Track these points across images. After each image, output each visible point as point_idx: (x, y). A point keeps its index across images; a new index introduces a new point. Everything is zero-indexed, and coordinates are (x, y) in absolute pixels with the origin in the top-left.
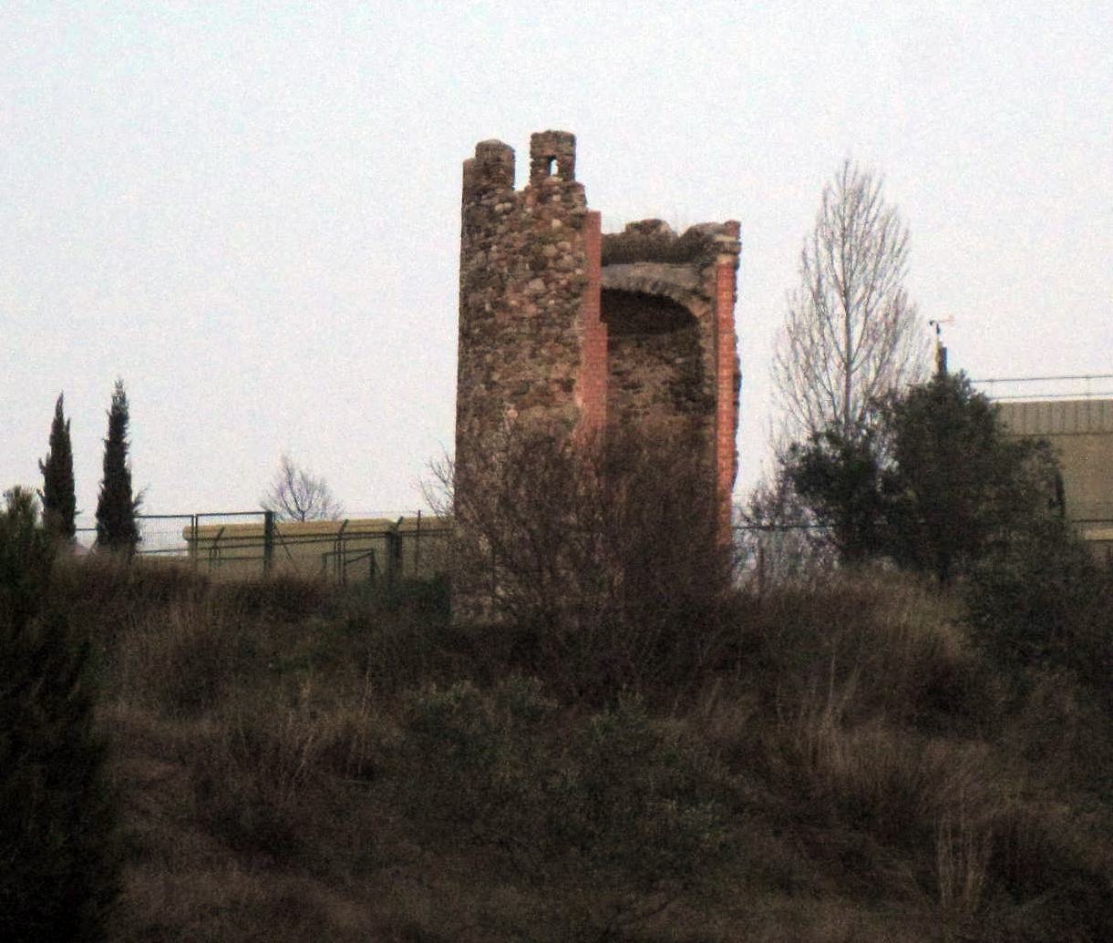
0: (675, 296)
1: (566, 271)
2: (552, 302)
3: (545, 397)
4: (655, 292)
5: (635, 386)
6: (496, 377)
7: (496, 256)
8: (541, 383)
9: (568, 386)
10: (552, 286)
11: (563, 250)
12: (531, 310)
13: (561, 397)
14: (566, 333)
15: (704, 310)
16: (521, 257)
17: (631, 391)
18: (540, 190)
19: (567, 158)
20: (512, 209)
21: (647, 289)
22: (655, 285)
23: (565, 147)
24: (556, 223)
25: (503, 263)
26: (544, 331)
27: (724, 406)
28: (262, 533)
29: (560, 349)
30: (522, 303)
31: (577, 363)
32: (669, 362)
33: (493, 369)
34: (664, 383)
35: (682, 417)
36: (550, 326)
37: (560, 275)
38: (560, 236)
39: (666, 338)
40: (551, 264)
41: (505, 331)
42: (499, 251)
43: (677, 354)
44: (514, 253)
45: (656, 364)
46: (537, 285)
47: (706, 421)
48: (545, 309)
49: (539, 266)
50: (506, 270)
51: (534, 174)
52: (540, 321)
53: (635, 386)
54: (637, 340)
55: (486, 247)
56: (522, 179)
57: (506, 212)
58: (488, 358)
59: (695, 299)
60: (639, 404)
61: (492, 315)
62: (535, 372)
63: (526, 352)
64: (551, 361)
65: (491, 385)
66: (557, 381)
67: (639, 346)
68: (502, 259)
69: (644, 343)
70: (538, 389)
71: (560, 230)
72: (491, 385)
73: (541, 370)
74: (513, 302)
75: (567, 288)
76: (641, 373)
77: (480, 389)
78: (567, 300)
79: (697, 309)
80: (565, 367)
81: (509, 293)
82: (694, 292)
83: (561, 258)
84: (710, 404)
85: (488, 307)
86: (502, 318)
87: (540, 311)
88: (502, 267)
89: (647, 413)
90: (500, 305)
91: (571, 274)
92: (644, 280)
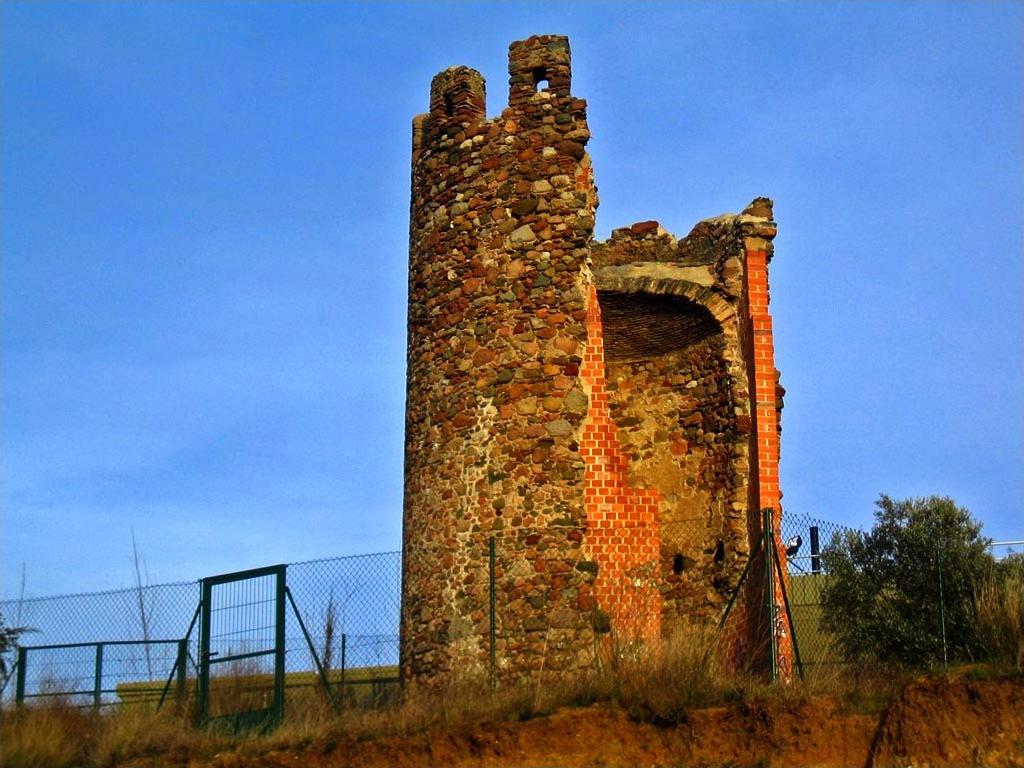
0: (691, 295)
1: (564, 213)
2: (547, 255)
3: (539, 383)
4: (663, 291)
5: (634, 422)
6: (465, 365)
7: (463, 206)
8: (532, 365)
9: (571, 367)
10: (546, 234)
11: (561, 185)
12: (516, 268)
13: (564, 383)
14: (566, 295)
15: (727, 313)
16: (500, 201)
17: (627, 428)
18: (527, 115)
19: (561, 67)
20: (486, 142)
21: (652, 288)
22: (661, 284)
23: (557, 54)
24: (549, 151)
25: (473, 214)
26: (535, 293)
27: (765, 428)
28: (396, 675)
29: (562, 317)
30: (502, 262)
31: (583, 336)
32: (680, 389)
33: (459, 354)
34: (671, 415)
35: (698, 454)
36: (546, 288)
37: (557, 219)
38: (554, 169)
39: (672, 359)
40: (542, 205)
41: (477, 301)
42: (466, 201)
43: (689, 377)
44: (489, 198)
45: (660, 393)
46: (525, 233)
47: (738, 451)
48: (534, 264)
49: (526, 211)
50: (477, 221)
51: (515, 93)
52: (527, 282)
53: (634, 422)
54: (632, 364)
55: (447, 200)
56: (497, 102)
57: (476, 147)
58: (454, 342)
59: (716, 296)
60: (638, 444)
61: (457, 284)
62: (524, 351)
63: (510, 325)
64: (544, 336)
65: (456, 376)
66: (555, 362)
67: (635, 372)
68: (470, 209)
69: (641, 368)
70: (528, 374)
71: (552, 161)
72: (456, 376)
73: (533, 347)
74: (488, 262)
75: (566, 236)
76: (642, 406)
77: (442, 386)
78: (567, 251)
79: (721, 311)
80: (567, 341)
81: (482, 250)
82: (714, 289)
83: (557, 196)
84: (748, 430)
85: (451, 275)
86: (477, 285)
87: (529, 268)
88: (471, 219)
89: (649, 455)
90: (471, 269)
91: (572, 216)
92: (647, 280)
